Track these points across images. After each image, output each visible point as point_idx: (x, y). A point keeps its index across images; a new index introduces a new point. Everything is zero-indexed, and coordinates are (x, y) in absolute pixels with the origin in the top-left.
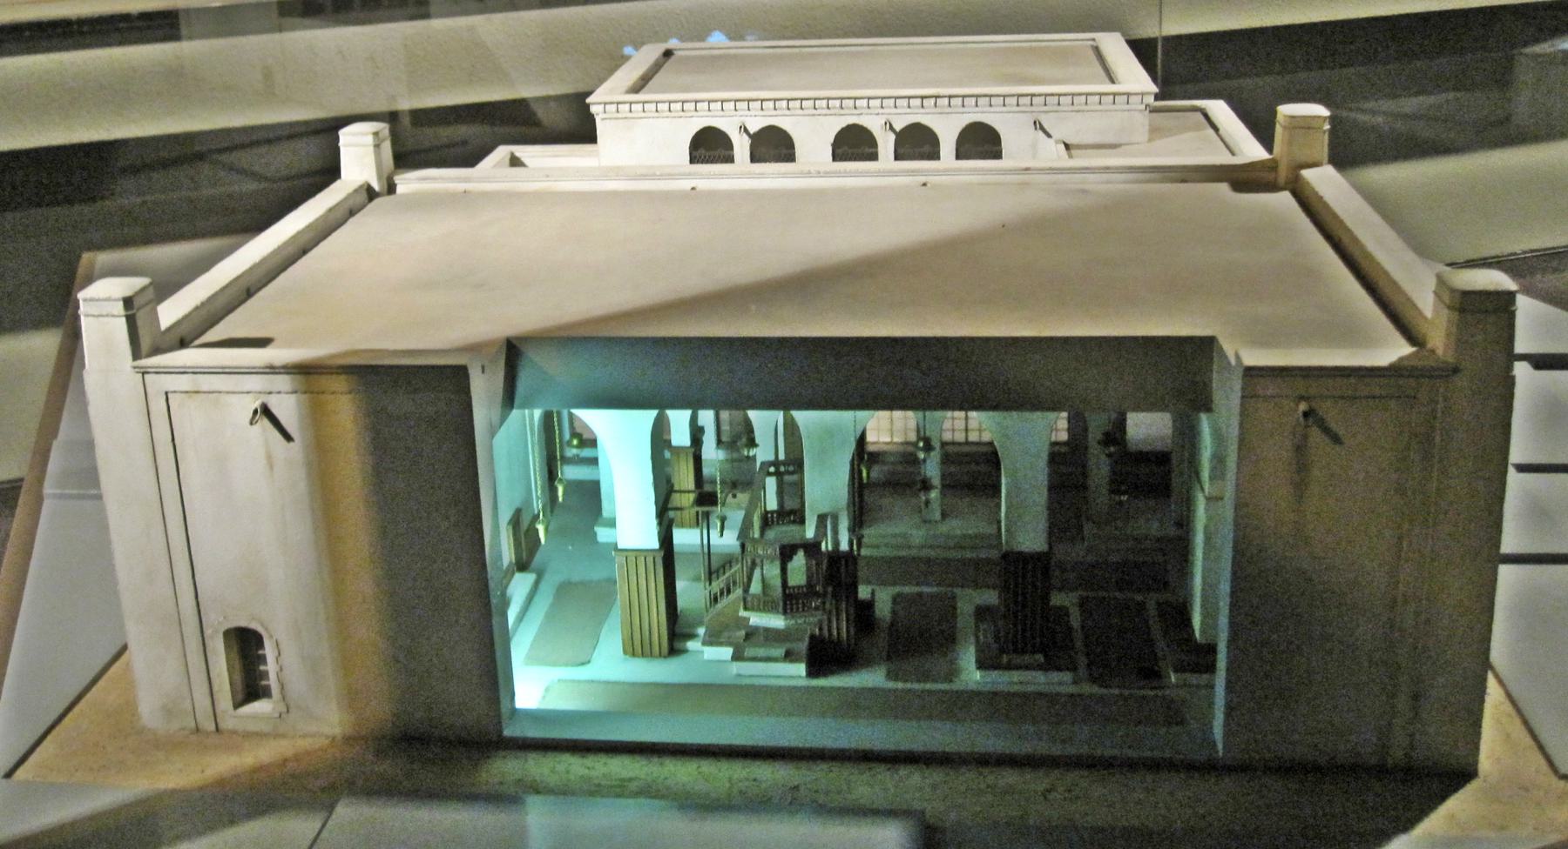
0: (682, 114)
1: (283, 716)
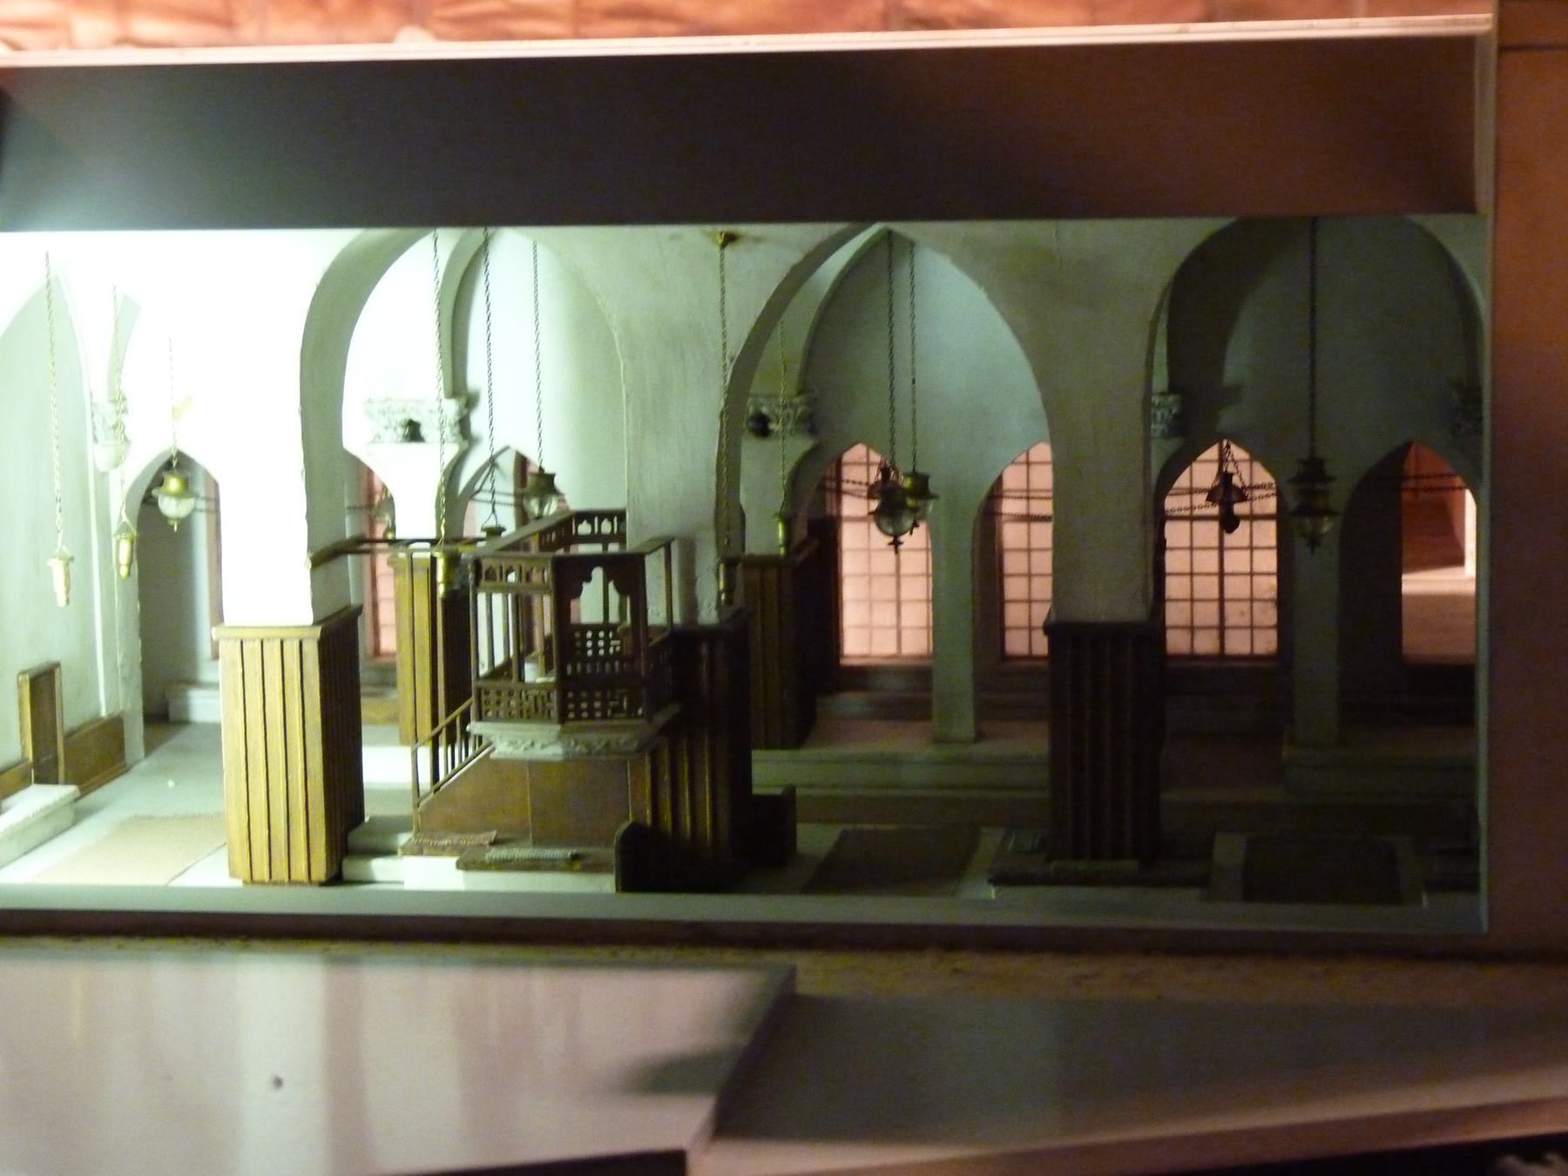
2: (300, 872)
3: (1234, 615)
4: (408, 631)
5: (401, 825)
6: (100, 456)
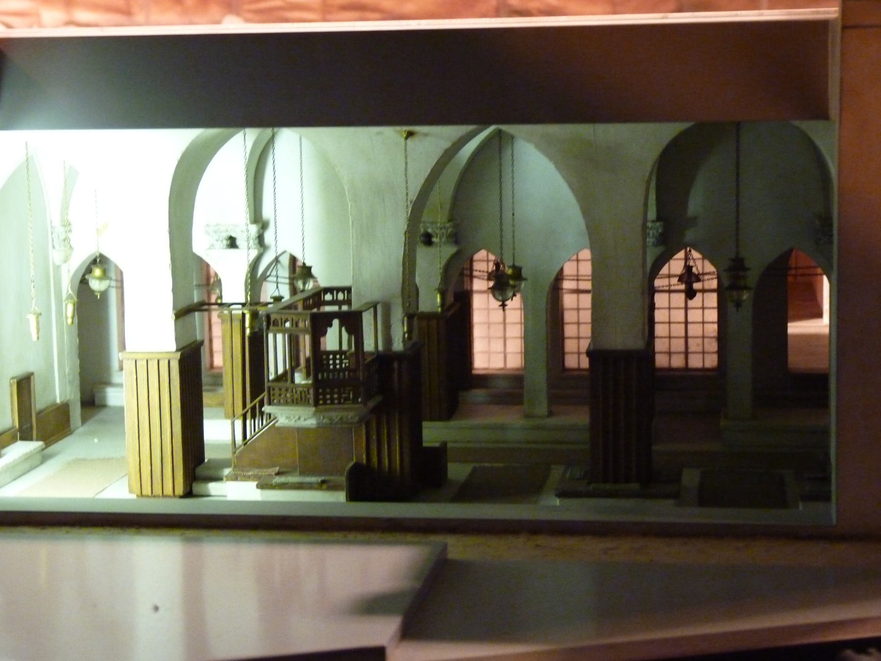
2: (169, 490)
3: (694, 345)
4: (229, 355)
5: (225, 464)
6: (56, 256)
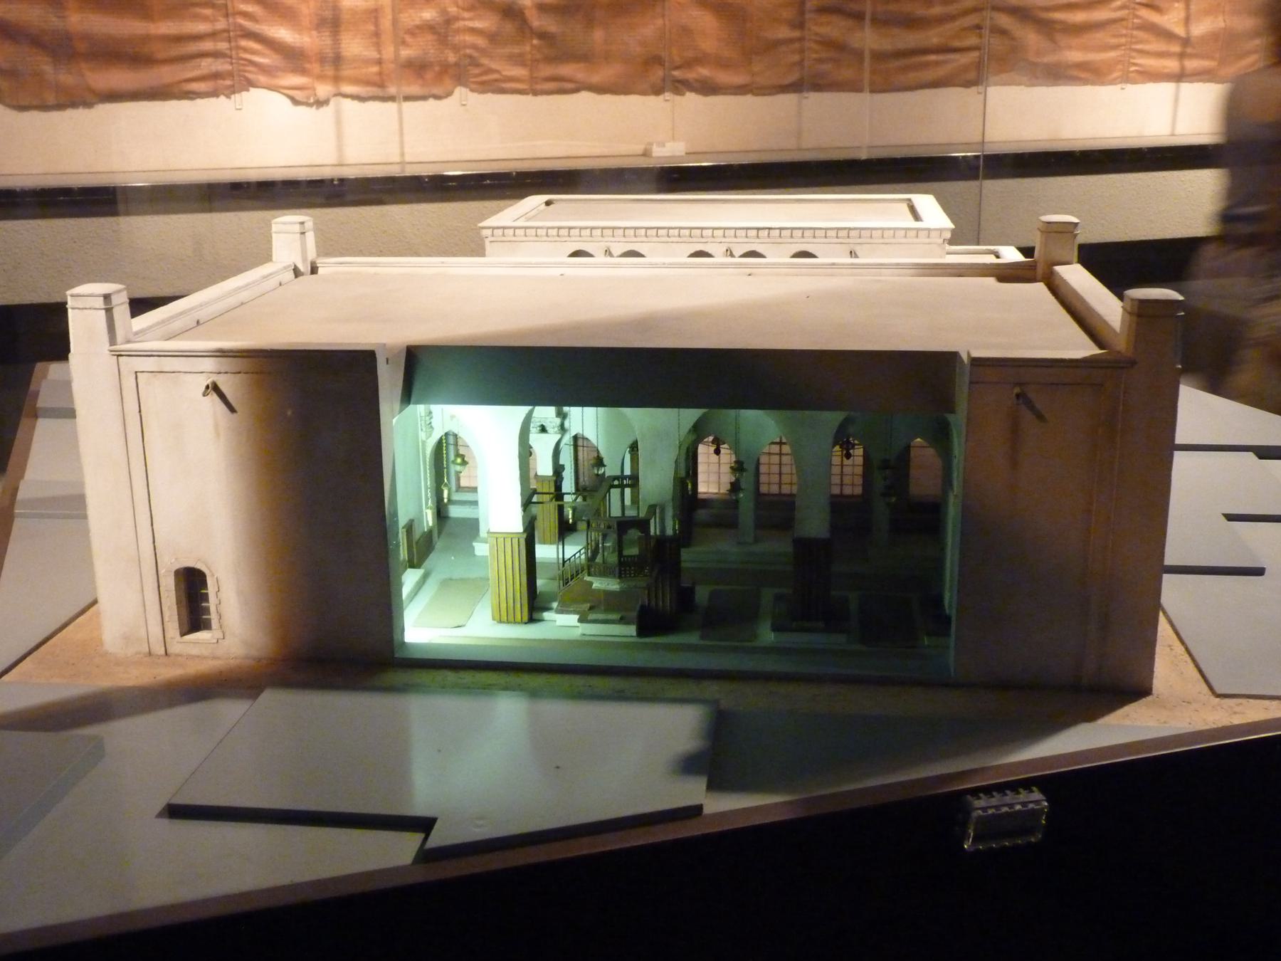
0: (557, 239)
1: (219, 641)
3: (847, 480)
4: (421, 265)
6: (422, 435)
